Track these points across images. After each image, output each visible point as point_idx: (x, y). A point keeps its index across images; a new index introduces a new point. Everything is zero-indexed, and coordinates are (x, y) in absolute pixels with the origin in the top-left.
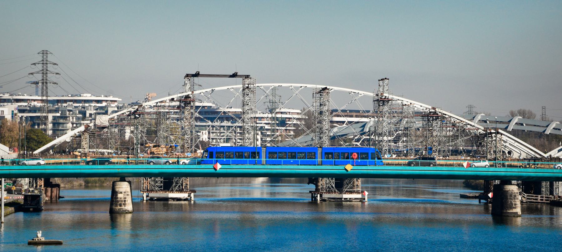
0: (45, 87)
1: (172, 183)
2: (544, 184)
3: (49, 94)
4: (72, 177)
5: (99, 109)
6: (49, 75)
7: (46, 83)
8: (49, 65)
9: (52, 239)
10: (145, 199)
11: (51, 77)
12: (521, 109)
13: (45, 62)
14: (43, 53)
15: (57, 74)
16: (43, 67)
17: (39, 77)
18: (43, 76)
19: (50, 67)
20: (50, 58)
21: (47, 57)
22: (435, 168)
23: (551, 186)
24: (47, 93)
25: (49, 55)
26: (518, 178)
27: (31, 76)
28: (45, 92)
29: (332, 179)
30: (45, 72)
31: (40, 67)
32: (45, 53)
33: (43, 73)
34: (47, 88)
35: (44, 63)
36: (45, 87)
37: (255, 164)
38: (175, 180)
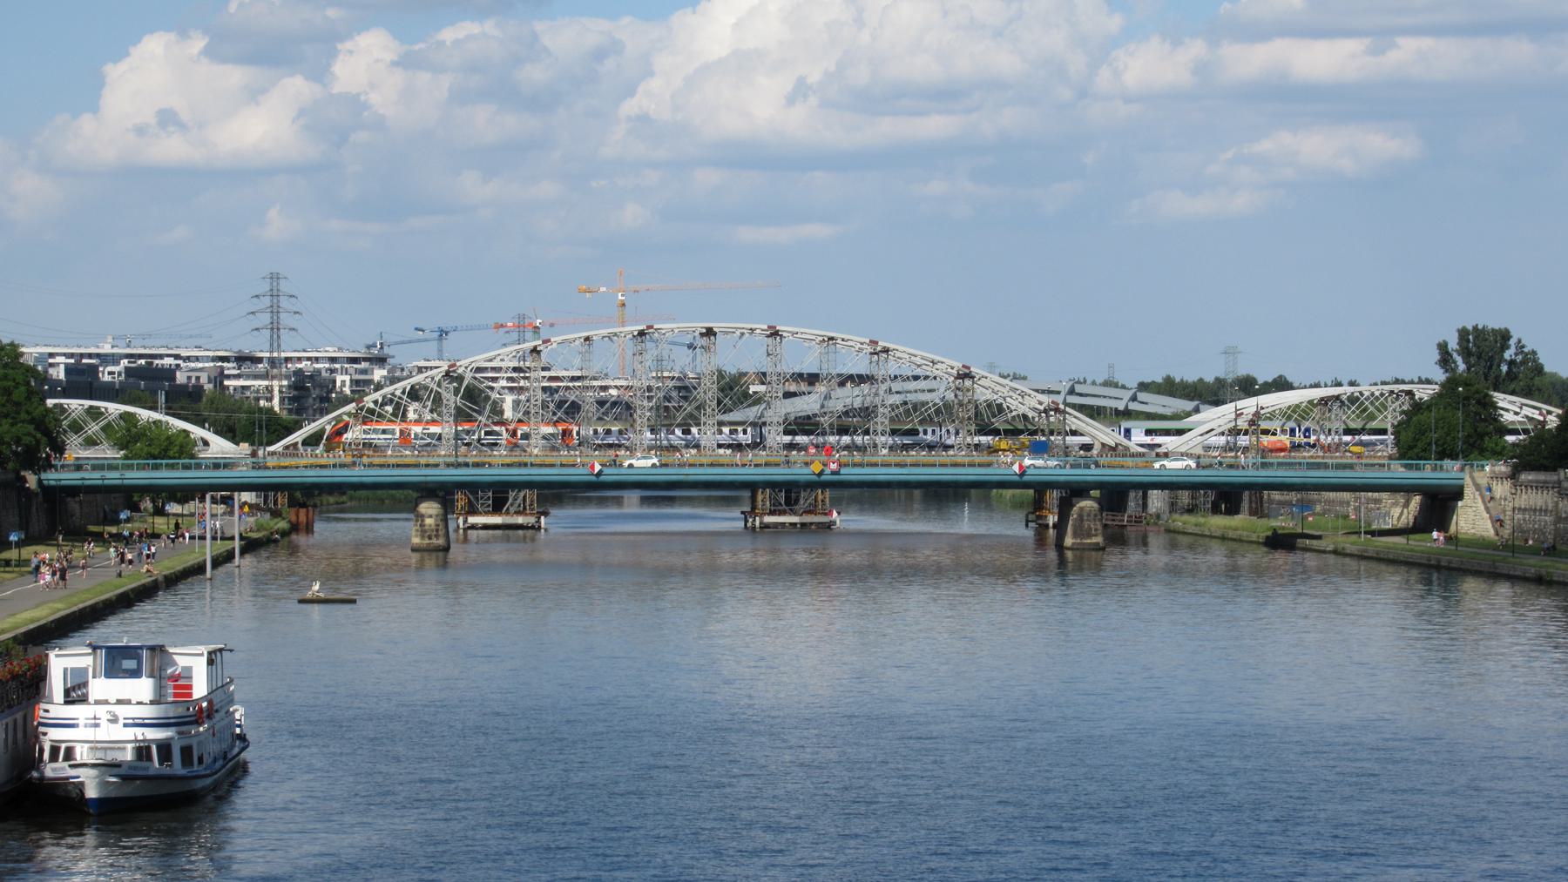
0: (275, 336)
1: (507, 499)
2: (1132, 494)
3: (282, 348)
4: (1378, 492)
5: (44, 378)
6: (282, 316)
7: (278, 329)
8: (281, 298)
9: (102, 594)
10: (461, 526)
11: (285, 319)
12: (1201, 380)
13: (275, 293)
14: (272, 278)
15: (296, 313)
16: (272, 301)
17: (265, 319)
18: (272, 317)
19: (285, 303)
20: (285, 287)
21: (278, 284)
22: (1099, 471)
23: (1145, 497)
24: (279, 346)
25: (282, 282)
26: (1100, 485)
27: (251, 316)
28: (275, 345)
29: (781, 491)
30: (275, 311)
31: (267, 301)
32: (275, 277)
33: (272, 312)
34: (279, 337)
35: (274, 294)
36: (275, 336)
37: (187, 467)
38: (512, 494)
